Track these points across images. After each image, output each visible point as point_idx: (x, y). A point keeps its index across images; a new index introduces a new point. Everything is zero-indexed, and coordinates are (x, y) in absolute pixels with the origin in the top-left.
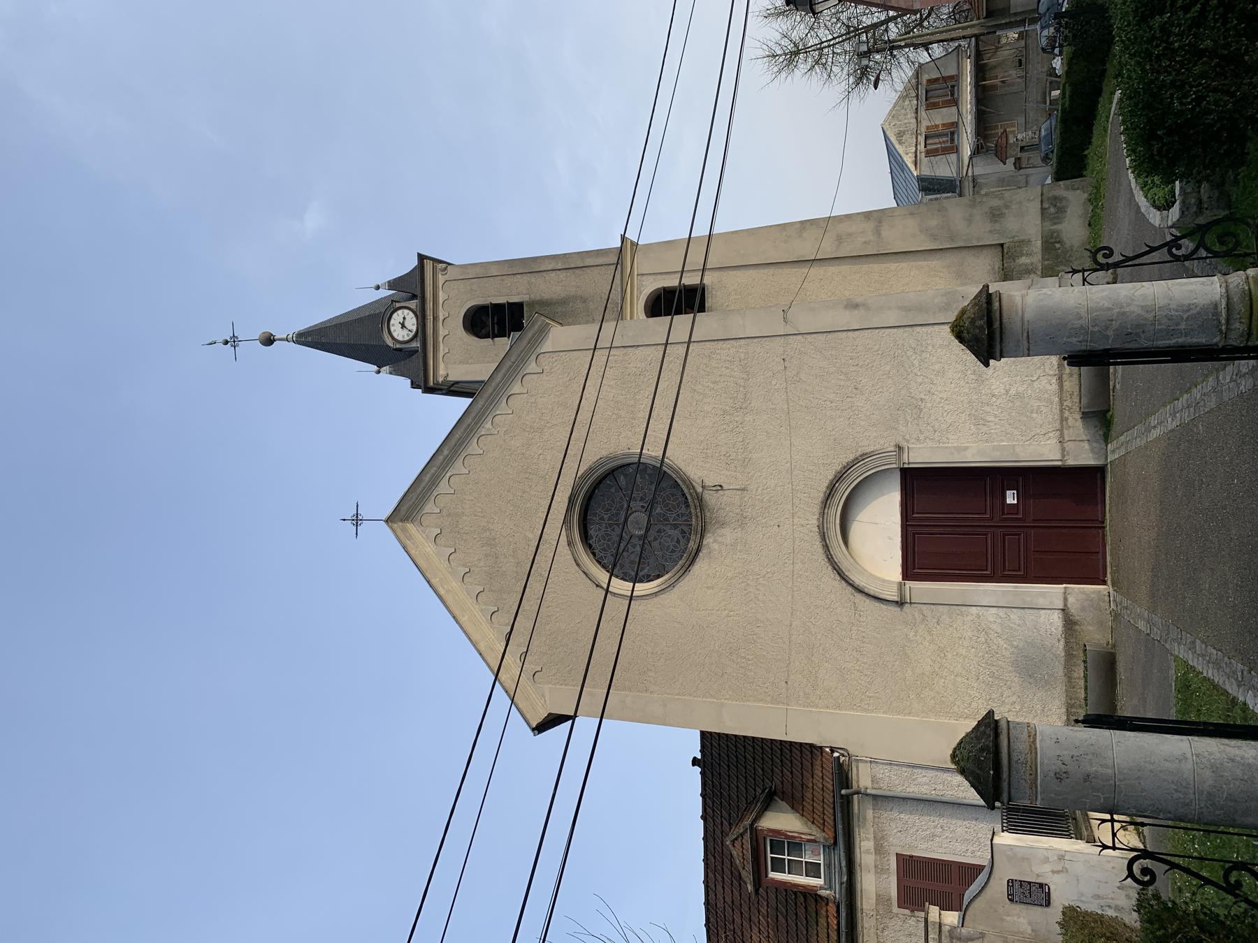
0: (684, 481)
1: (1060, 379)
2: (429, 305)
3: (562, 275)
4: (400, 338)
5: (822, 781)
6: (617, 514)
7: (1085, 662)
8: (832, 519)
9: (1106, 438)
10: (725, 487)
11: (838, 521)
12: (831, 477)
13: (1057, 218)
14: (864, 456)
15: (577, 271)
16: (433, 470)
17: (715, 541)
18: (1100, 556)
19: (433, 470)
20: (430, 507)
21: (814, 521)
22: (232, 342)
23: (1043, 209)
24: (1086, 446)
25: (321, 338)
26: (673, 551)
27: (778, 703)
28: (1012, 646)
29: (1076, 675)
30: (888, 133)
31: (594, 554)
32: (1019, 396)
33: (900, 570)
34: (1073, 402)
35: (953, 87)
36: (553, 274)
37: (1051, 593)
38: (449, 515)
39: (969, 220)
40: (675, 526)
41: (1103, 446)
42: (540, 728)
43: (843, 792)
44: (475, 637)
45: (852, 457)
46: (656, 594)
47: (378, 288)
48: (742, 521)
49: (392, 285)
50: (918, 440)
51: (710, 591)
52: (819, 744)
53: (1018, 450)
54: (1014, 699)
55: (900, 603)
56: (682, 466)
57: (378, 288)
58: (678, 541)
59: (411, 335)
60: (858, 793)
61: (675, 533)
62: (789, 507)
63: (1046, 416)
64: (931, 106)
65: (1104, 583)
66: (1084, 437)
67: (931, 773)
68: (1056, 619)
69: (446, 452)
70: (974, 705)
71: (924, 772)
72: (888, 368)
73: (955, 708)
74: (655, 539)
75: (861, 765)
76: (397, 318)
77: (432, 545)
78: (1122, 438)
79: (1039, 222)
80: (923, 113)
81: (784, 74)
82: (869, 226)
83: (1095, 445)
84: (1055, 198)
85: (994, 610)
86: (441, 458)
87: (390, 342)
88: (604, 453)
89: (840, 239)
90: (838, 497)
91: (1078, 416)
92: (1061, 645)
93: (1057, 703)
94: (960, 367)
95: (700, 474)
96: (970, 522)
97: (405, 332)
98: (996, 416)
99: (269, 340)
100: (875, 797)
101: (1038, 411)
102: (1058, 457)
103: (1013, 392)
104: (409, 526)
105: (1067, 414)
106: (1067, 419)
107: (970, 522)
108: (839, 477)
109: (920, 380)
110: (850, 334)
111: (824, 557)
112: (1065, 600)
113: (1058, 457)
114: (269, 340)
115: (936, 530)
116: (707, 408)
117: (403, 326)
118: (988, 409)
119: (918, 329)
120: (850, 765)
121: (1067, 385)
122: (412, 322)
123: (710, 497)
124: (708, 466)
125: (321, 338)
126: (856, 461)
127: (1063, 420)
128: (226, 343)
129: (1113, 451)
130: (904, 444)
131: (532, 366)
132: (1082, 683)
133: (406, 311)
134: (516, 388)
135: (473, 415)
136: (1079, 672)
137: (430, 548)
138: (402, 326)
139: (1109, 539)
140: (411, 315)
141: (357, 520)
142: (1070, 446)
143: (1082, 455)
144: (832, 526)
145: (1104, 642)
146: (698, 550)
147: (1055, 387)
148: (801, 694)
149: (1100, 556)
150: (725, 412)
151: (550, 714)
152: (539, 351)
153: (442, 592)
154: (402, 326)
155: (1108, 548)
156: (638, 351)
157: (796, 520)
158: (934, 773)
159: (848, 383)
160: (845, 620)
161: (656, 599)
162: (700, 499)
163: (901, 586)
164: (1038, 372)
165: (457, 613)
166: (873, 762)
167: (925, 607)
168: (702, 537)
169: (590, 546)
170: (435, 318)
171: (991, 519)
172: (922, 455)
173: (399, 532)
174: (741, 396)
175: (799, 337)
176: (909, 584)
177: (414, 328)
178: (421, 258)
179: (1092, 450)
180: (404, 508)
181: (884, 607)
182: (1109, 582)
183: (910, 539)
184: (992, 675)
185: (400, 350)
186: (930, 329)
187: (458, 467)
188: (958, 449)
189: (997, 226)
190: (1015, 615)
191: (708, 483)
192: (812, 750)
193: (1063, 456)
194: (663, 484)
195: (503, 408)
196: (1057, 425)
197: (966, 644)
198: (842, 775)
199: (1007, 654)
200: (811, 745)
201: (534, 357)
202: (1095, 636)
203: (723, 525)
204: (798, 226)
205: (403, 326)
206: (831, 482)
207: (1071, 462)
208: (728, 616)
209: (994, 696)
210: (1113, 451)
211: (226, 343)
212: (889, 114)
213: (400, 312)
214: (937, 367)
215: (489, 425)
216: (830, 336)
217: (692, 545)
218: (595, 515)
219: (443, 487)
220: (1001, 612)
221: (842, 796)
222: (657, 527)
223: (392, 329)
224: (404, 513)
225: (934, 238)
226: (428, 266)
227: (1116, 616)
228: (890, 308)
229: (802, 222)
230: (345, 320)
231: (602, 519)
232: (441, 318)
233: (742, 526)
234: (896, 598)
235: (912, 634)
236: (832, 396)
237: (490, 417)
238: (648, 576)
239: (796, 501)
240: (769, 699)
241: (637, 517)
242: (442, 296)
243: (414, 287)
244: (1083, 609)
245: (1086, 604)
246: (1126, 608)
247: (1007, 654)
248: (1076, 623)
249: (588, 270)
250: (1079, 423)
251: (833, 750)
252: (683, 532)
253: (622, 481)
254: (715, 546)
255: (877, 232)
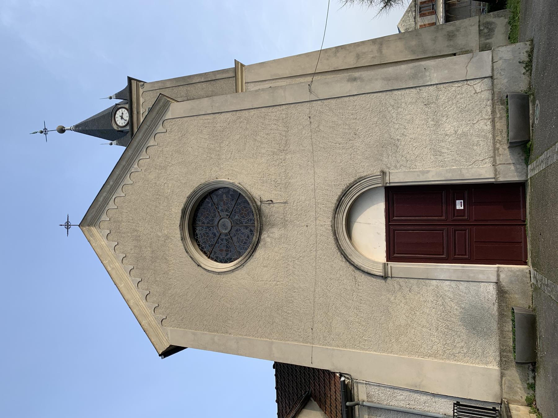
0: (249, 198)
1: (493, 122)
2: (135, 105)
3: (204, 85)
4: (121, 125)
5: (336, 394)
6: (213, 220)
7: (513, 321)
8: (340, 221)
9: (527, 162)
10: (274, 201)
11: (344, 223)
12: (339, 194)
13: (489, 35)
14: (361, 179)
15: (212, 82)
16: (104, 194)
17: (268, 236)
18: (523, 245)
19: (104, 194)
20: (104, 217)
21: (329, 223)
22: (44, 132)
23: (480, 31)
24: (512, 167)
25: (85, 128)
26: (245, 243)
27: (307, 343)
28: (461, 308)
29: (506, 329)
30: (400, 29)
31: (199, 245)
32: (464, 134)
33: (385, 255)
34: (502, 137)
35: (433, 5)
36: (199, 85)
37: (488, 271)
38: (114, 222)
39: (435, 40)
40: (247, 227)
41: (525, 167)
42: (167, 353)
43: (348, 404)
44: (128, 297)
45: (352, 180)
46: (233, 271)
47: (111, 98)
48: (285, 224)
49: (118, 96)
50: (396, 167)
51: (265, 269)
52: (333, 371)
53: (464, 171)
54: (463, 344)
55: (385, 277)
56: (248, 189)
57: (111, 98)
58: (248, 237)
59: (126, 122)
60: (358, 404)
61: (247, 231)
62: (314, 213)
63: (483, 148)
64: (422, 15)
65: (525, 263)
66: (511, 161)
67: (406, 393)
68: (492, 289)
69: (111, 183)
70: (435, 347)
71: (401, 392)
72: (376, 119)
73: (422, 349)
74: (235, 236)
75: (359, 385)
76: (119, 113)
77: (105, 240)
78: (542, 157)
79: (477, 38)
80: (418, 19)
81: (352, 5)
82: (375, 48)
83: (518, 166)
84: (488, 23)
85: (448, 283)
86: (109, 186)
87: (115, 127)
88: (203, 181)
89: (358, 57)
90: (343, 208)
91: (506, 147)
92: (496, 307)
93: (493, 348)
94: (424, 117)
95: (259, 193)
96: (433, 221)
97: (123, 121)
98: (448, 149)
99: (62, 130)
100: (369, 407)
101: (478, 144)
102: (492, 176)
103: (460, 132)
104: (93, 229)
105: (498, 145)
106: (498, 149)
107: (433, 221)
108: (345, 194)
109: (397, 126)
110: (351, 98)
111: (335, 246)
112: (498, 276)
113: (492, 176)
114: (62, 130)
115: (409, 227)
116: (263, 151)
117: (122, 118)
118: (443, 144)
119: (396, 92)
120: (352, 385)
121: (498, 125)
122: (126, 116)
123: (265, 209)
124: (264, 188)
125: (85, 128)
126: (355, 182)
127: (495, 149)
128: (42, 132)
129: (533, 170)
130: (387, 170)
131: (160, 129)
132: (511, 335)
133: (123, 110)
134: (151, 142)
135: (126, 160)
136: (509, 327)
137: (104, 242)
138: (121, 119)
139: (529, 233)
140: (126, 111)
141: (68, 226)
142: (500, 168)
143: (510, 174)
144: (340, 226)
145: (526, 306)
146: (258, 242)
147: (489, 127)
148: (321, 336)
149: (523, 245)
150: (274, 153)
151: (171, 346)
152: (164, 118)
153: (109, 269)
154: (121, 119)
155: (528, 240)
156: (222, 116)
157: (318, 222)
158: (408, 393)
159: (350, 131)
160: (349, 288)
161: (233, 274)
162: (259, 210)
163: (385, 265)
164: (478, 117)
165: (117, 282)
166: (367, 384)
167: (401, 280)
168: (260, 234)
169: (197, 240)
170: (138, 113)
171: (446, 220)
172: (400, 177)
173: (86, 233)
174: (283, 142)
175: (319, 102)
176: (391, 264)
177: (128, 119)
178: (130, 79)
179: (517, 169)
180: (89, 218)
181: (374, 279)
182: (530, 263)
183: (391, 234)
184: (447, 327)
185: (122, 131)
186: (403, 92)
187: (119, 192)
188: (423, 173)
189: (452, 43)
190: (463, 286)
191: (265, 199)
192: (328, 375)
193: (496, 175)
194: (239, 201)
195: (144, 155)
196: (491, 154)
197: (429, 305)
198: (348, 392)
199: (457, 313)
200: (328, 371)
201: (161, 122)
202: (521, 302)
203: (273, 225)
204: (334, 50)
205: (122, 118)
206: (340, 196)
207: (502, 179)
208: (276, 285)
209: (448, 342)
210: (533, 170)
211: (42, 132)
212: (401, 20)
213: (120, 110)
214: (408, 117)
215: (136, 166)
216: (339, 100)
217: (255, 239)
218: (199, 221)
219: (111, 205)
220: (453, 284)
221: (347, 407)
222: (236, 228)
223: (117, 120)
224: (90, 220)
225: (413, 52)
226: (134, 84)
227: (536, 289)
228: (377, 79)
229: (337, 48)
230: (100, 116)
231: (203, 223)
232: (141, 112)
233: (285, 226)
234: (381, 274)
235: (393, 298)
236: (340, 140)
237: (137, 160)
238: (231, 259)
239: (318, 210)
240: (301, 339)
241: (222, 222)
242: (142, 100)
243: (128, 95)
244: (511, 282)
245: (513, 279)
246: (547, 285)
247: (457, 313)
248: (506, 292)
249: (218, 82)
250: (507, 152)
251: (341, 375)
252: (251, 231)
253: (215, 200)
254: (268, 240)
255: (380, 51)
